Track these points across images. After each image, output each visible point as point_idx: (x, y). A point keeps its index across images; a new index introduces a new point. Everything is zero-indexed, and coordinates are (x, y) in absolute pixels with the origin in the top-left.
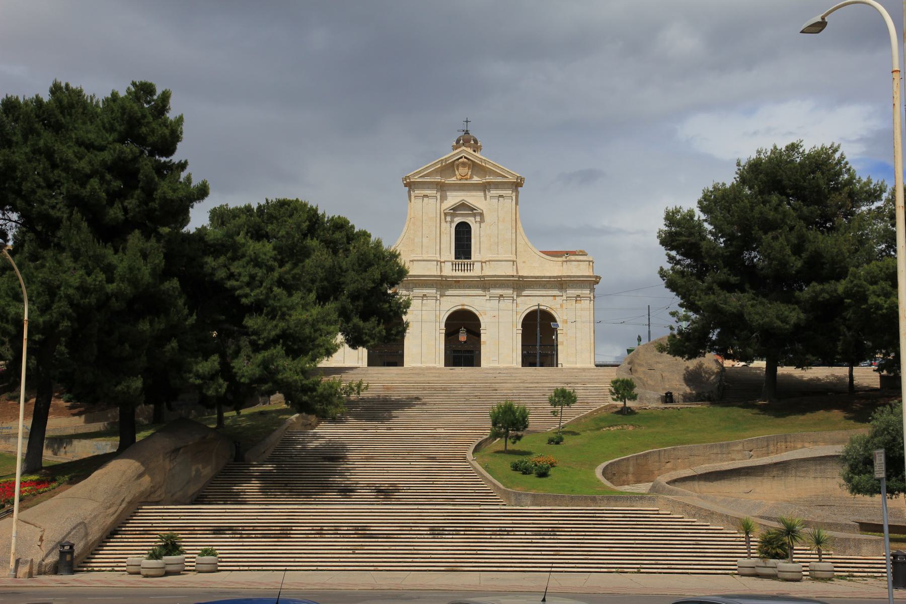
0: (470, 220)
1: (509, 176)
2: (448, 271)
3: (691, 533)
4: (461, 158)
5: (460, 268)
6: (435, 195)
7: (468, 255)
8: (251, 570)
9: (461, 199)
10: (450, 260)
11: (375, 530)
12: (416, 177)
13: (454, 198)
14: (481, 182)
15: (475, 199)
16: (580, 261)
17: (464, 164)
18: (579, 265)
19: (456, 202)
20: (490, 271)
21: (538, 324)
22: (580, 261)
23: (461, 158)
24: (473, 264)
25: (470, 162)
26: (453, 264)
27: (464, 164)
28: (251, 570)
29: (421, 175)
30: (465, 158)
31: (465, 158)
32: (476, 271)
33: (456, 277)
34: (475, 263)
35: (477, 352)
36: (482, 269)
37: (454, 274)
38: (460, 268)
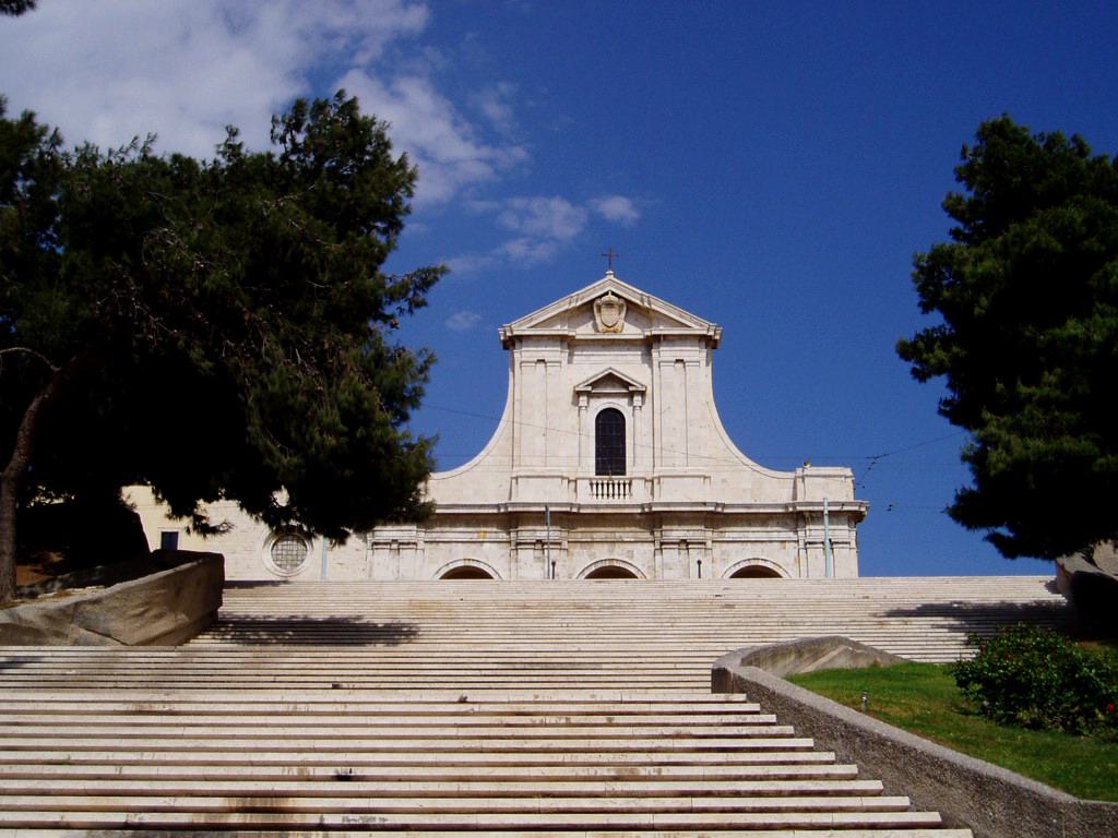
0: (621, 404)
1: (692, 325)
2: (586, 497)
3: (673, 750)
4: (607, 294)
5: (605, 492)
6: (558, 359)
7: (620, 468)
8: (68, 826)
9: (607, 366)
10: (586, 475)
11: (128, 642)
12: (523, 328)
13: (591, 365)
14: (642, 337)
15: (629, 365)
16: (830, 476)
17: (610, 305)
18: (827, 484)
19: (597, 372)
20: (673, 495)
21: (26, 422)
22: (830, 476)
23: (607, 294)
24: (630, 484)
25: (622, 302)
26: (591, 484)
27: (610, 305)
28: (68, 826)
29: (533, 323)
30: (613, 294)
31: (613, 294)
32: (638, 496)
33: (596, 507)
34: (634, 482)
35: (963, 749)
36: (652, 494)
37: (594, 501)
38: (605, 492)
